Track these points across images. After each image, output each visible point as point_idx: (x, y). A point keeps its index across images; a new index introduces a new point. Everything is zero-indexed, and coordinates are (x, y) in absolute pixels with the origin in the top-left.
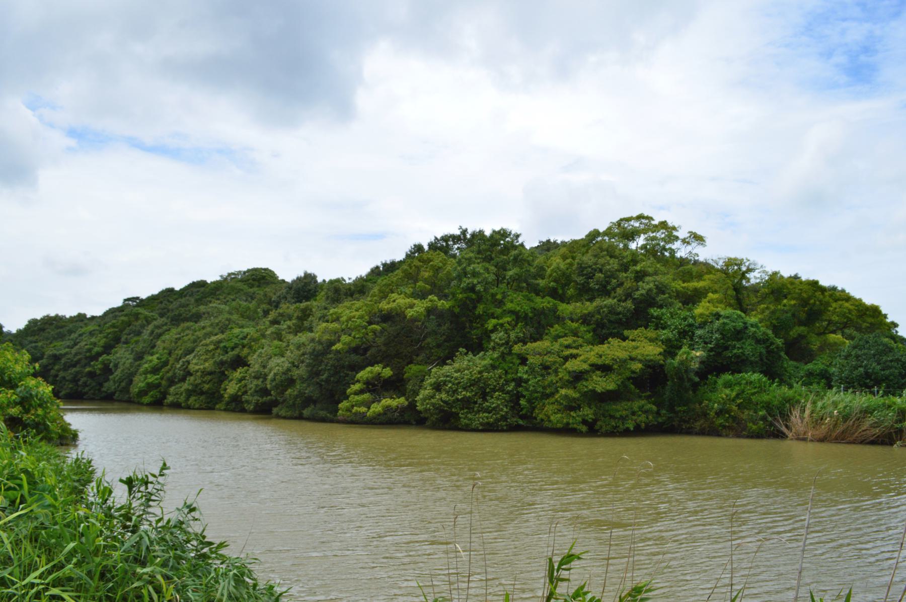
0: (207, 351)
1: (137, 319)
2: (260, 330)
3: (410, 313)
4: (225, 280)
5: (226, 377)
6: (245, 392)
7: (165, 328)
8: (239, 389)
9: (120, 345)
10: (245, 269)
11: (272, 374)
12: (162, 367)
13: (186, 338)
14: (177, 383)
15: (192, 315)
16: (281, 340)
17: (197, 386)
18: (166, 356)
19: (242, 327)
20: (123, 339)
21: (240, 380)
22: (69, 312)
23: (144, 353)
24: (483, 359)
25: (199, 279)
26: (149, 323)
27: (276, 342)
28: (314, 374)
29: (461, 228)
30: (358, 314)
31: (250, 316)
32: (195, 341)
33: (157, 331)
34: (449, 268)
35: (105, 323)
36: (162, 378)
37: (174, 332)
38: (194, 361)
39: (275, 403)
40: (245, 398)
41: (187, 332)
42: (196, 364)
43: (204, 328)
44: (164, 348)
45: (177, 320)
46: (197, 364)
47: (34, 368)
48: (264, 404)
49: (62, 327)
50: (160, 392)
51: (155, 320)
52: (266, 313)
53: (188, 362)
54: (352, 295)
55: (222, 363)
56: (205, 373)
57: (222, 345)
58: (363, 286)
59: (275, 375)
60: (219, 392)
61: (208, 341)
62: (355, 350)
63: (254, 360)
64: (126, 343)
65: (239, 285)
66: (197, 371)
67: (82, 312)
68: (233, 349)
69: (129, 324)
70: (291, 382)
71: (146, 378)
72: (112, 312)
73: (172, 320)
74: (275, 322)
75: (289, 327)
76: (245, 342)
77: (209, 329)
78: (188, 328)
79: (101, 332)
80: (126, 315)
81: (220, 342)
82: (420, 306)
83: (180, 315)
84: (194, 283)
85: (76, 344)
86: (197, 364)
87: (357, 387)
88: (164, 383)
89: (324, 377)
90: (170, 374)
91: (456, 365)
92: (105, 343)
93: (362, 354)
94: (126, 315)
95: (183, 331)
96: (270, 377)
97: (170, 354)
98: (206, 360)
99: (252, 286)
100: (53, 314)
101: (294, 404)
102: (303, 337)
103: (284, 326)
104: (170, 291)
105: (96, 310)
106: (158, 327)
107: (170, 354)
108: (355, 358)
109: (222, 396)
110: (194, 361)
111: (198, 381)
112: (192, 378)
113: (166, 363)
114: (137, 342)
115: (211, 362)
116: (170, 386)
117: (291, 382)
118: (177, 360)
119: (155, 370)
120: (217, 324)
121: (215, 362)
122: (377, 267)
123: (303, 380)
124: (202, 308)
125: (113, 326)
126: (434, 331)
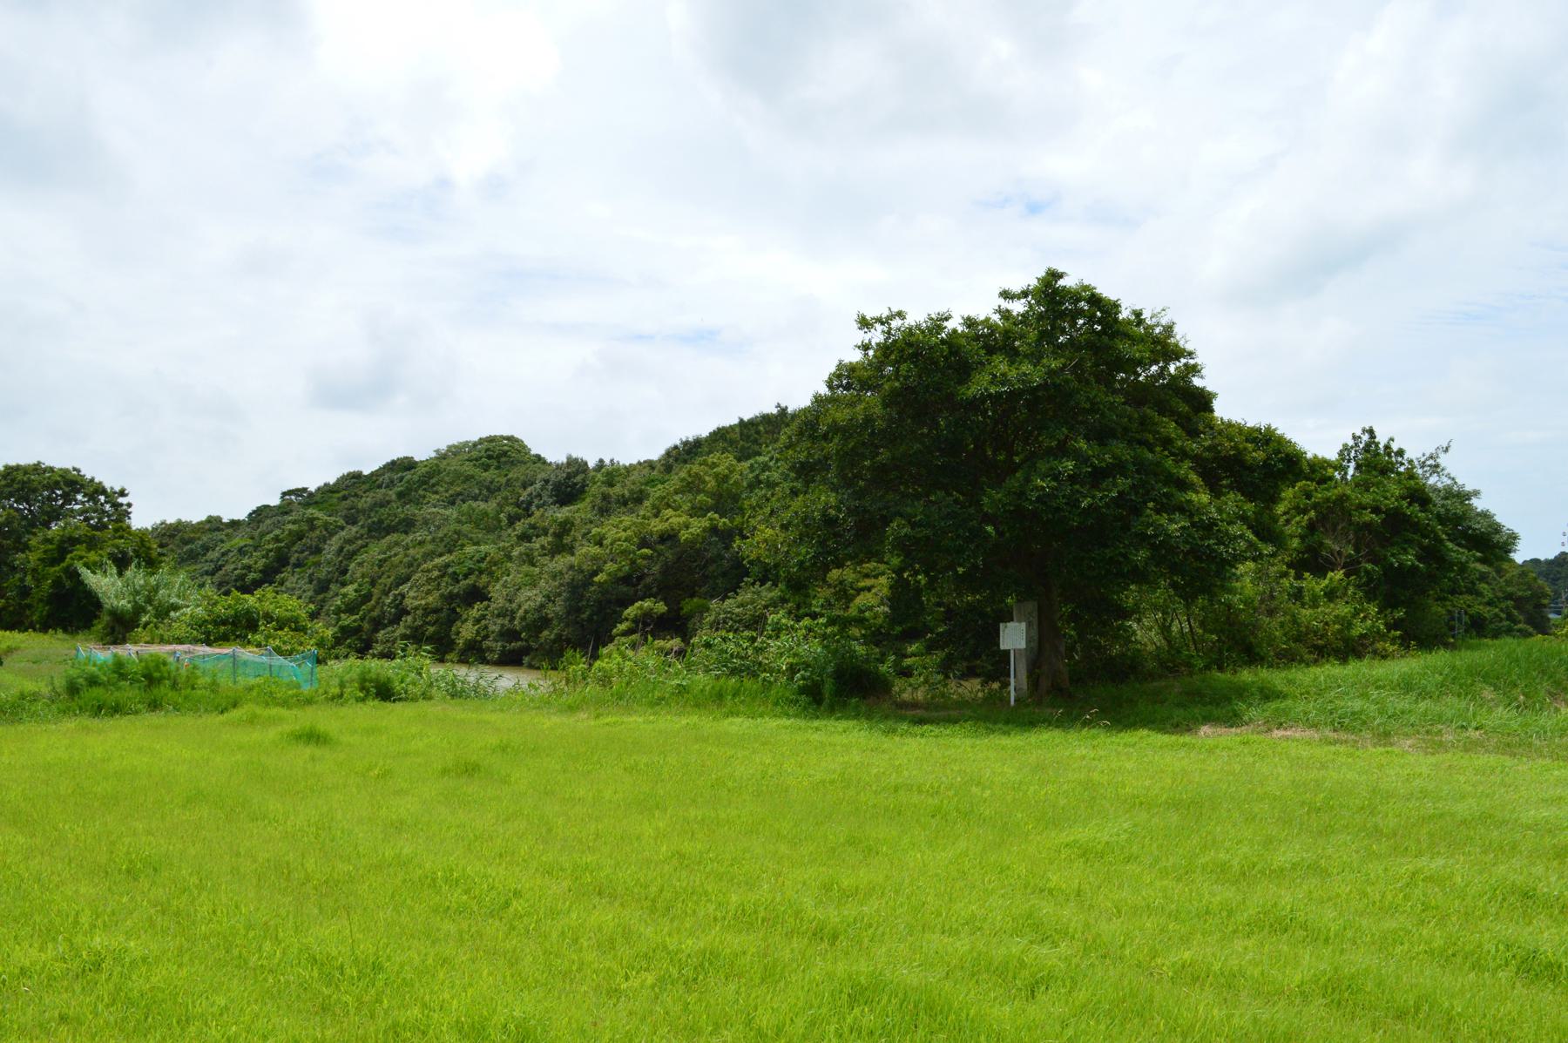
0: (429, 580)
1: (313, 528)
2: (504, 549)
3: (684, 536)
4: (442, 457)
5: (458, 616)
6: (486, 637)
7: (360, 542)
8: (478, 633)
9: (289, 568)
10: (476, 439)
11: (521, 612)
12: (363, 603)
13: (396, 560)
14: (385, 626)
15: (400, 523)
16: (534, 565)
17: (416, 629)
18: (367, 586)
19: (477, 544)
20: (293, 560)
21: (478, 621)
22: (196, 516)
23: (329, 581)
24: (770, 590)
25: (401, 455)
26: (332, 535)
27: (525, 568)
28: (573, 610)
29: (778, 406)
30: (623, 535)
31: (491, 527)
32: (410, 565)
33: (348, 547)
34: (736, 476)
35: (262, 535)
36: (362, 619)
37: (375, 551)
38: (412, 594)
39: (526, 651)
40: (486, 644)
41: (396, 549)
42: (415, 598)
43: (421, 543)
44: (363, 576)
45: (379, 530)
46: (415, 597)
47: (1292, 536)
48: (512, 652)
49: (191, 541)
50: (360, 639)
51: (342, 528)
52: (512, 520)
53: (403, 596)
54: (625, 504)
55: (450, 598)
56: (427, 611)
57: (450, 570)
58: (641, 491)
59: (526, 612)
60: (448, 636)
61: (429, 565)
62: (626, 580)
63: (497, 592)
64: (299, 564)
65: (468, 469)
66: (416, 608)
67: (214, 514)
68: (466, 576)
69: (300, 536)
70: (545, 622)
71: (339, 619)
72: (260, 514)
73: (370, 531)
74: (525, 537)
75: (543, 547)
76: (483, 565)
77: (430, 547)
78: (397, 544)
79: (256, 548)
80: (294, 522)
81: (447, 566)
82: (698, 525)
83: (381, 522)
84: (393, 463)
85: (220, 568)
86: (415, 597)
87: (622, 627)
88: (366, 626)
89: (584, 616)
90: (375, 614)
91: (739, 598)
92: (266, 566)
93: (631, 584)
94: (294, 522)
95: (389, 548)
96: (520, 613)
97: (373, 583)
98: (429, 592)
99: (486, 468)
100: (171, 520)
101: (551, 650)
102: (562, 562)
103: (536, 544)
104: (356, 477)
105: (237, 509)
106: (349, 541)
107: (373, 583)
108: (624, 588)
109: (453, 642)
110: (412, 594)
111: (419, 623)
112: (409, 618)
113: (367, 598)
114: (318, 564)
115: (436, 594)
116: (376, 630)
117: (545, 622)
118: (387, 594)
119: (351, 608)
120: (442, 540)
121: (442, 596)
122: (676, 447)
123: (560, 619)
124: (410, 510)
125: (277, 539)
126: (296, 620)
